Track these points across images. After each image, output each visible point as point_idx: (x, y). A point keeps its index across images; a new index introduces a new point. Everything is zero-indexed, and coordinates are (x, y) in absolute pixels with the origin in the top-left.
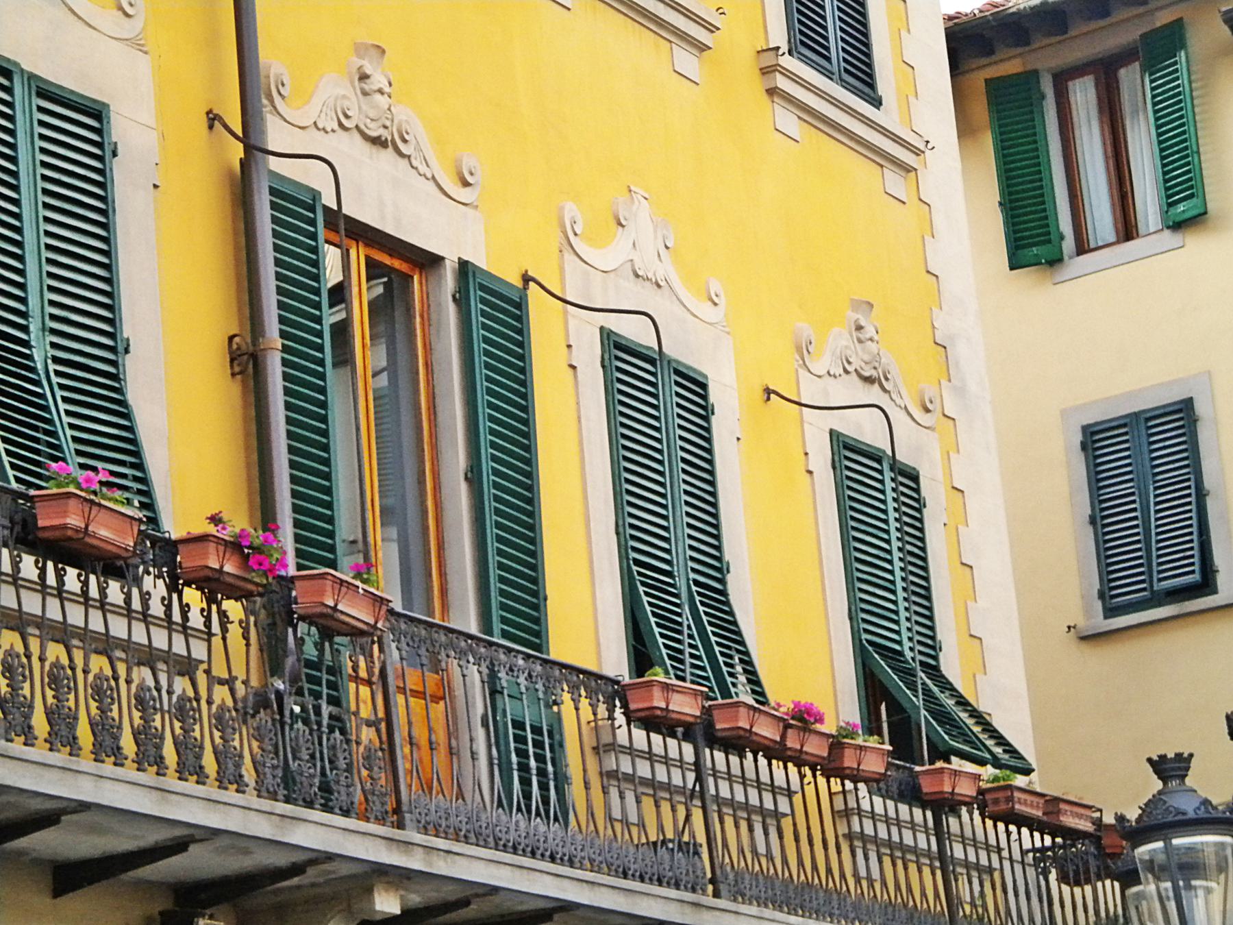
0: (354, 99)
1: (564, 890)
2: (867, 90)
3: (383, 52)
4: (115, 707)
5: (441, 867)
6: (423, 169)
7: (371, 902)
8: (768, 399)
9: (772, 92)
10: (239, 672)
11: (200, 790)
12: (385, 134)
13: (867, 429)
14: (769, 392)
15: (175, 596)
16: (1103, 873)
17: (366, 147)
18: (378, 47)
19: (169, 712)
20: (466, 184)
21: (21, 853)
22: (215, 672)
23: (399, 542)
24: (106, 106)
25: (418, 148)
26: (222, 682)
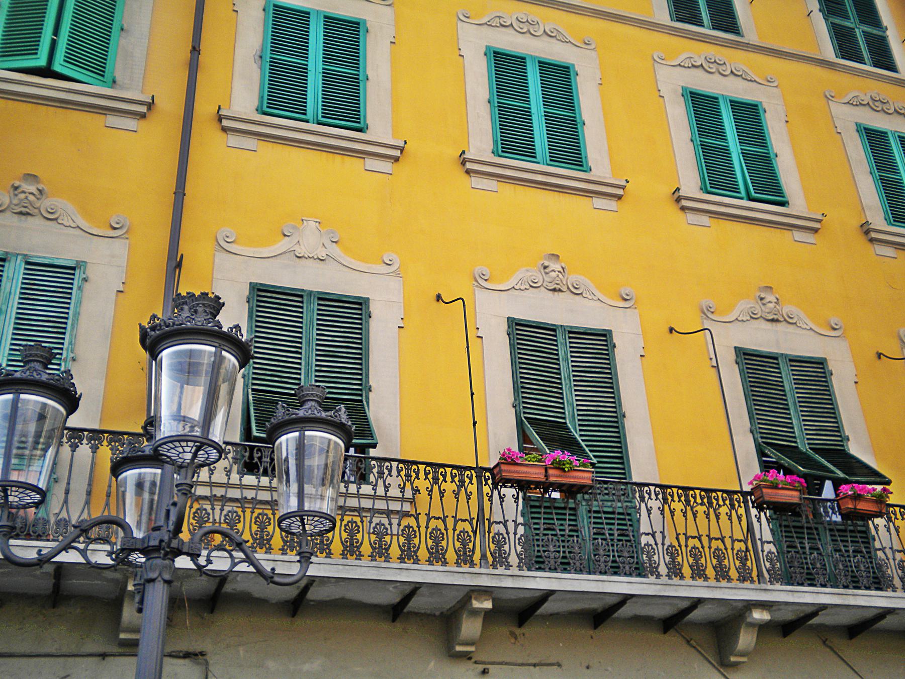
0: (757, 307)
1: (799, 597)
2: (101, 78)
3: (558, 256)
4: (889, 571)
5: (852, 601)
6: (805, 326)
7: (471, 604)
8: (880, 358)
9: (468, 172)
10: (510, 517)
11: (752, 586)
12: (776, 317)
13: (764, 339)
14: (879, 355)
15: (891, 524)
16: (328, 482)
17: (769, 324)
18: (767, 287)
19: (398, 535)
20: (834, 329)
21: (811, 625)
22: (895, 548)
23: (18, 393)
24: (825, 359)
25: (799, 318)
26: (879, 549)
